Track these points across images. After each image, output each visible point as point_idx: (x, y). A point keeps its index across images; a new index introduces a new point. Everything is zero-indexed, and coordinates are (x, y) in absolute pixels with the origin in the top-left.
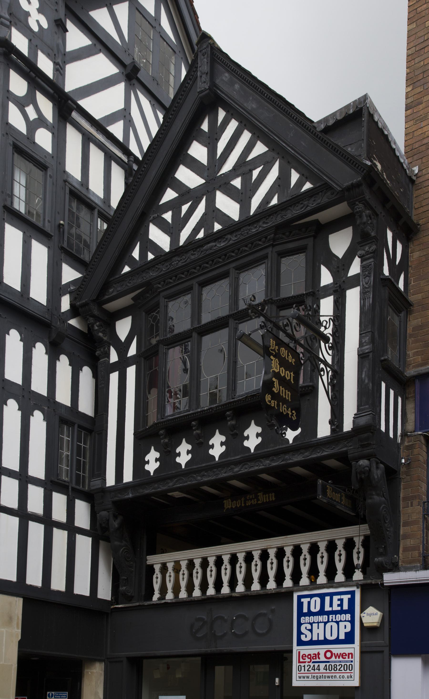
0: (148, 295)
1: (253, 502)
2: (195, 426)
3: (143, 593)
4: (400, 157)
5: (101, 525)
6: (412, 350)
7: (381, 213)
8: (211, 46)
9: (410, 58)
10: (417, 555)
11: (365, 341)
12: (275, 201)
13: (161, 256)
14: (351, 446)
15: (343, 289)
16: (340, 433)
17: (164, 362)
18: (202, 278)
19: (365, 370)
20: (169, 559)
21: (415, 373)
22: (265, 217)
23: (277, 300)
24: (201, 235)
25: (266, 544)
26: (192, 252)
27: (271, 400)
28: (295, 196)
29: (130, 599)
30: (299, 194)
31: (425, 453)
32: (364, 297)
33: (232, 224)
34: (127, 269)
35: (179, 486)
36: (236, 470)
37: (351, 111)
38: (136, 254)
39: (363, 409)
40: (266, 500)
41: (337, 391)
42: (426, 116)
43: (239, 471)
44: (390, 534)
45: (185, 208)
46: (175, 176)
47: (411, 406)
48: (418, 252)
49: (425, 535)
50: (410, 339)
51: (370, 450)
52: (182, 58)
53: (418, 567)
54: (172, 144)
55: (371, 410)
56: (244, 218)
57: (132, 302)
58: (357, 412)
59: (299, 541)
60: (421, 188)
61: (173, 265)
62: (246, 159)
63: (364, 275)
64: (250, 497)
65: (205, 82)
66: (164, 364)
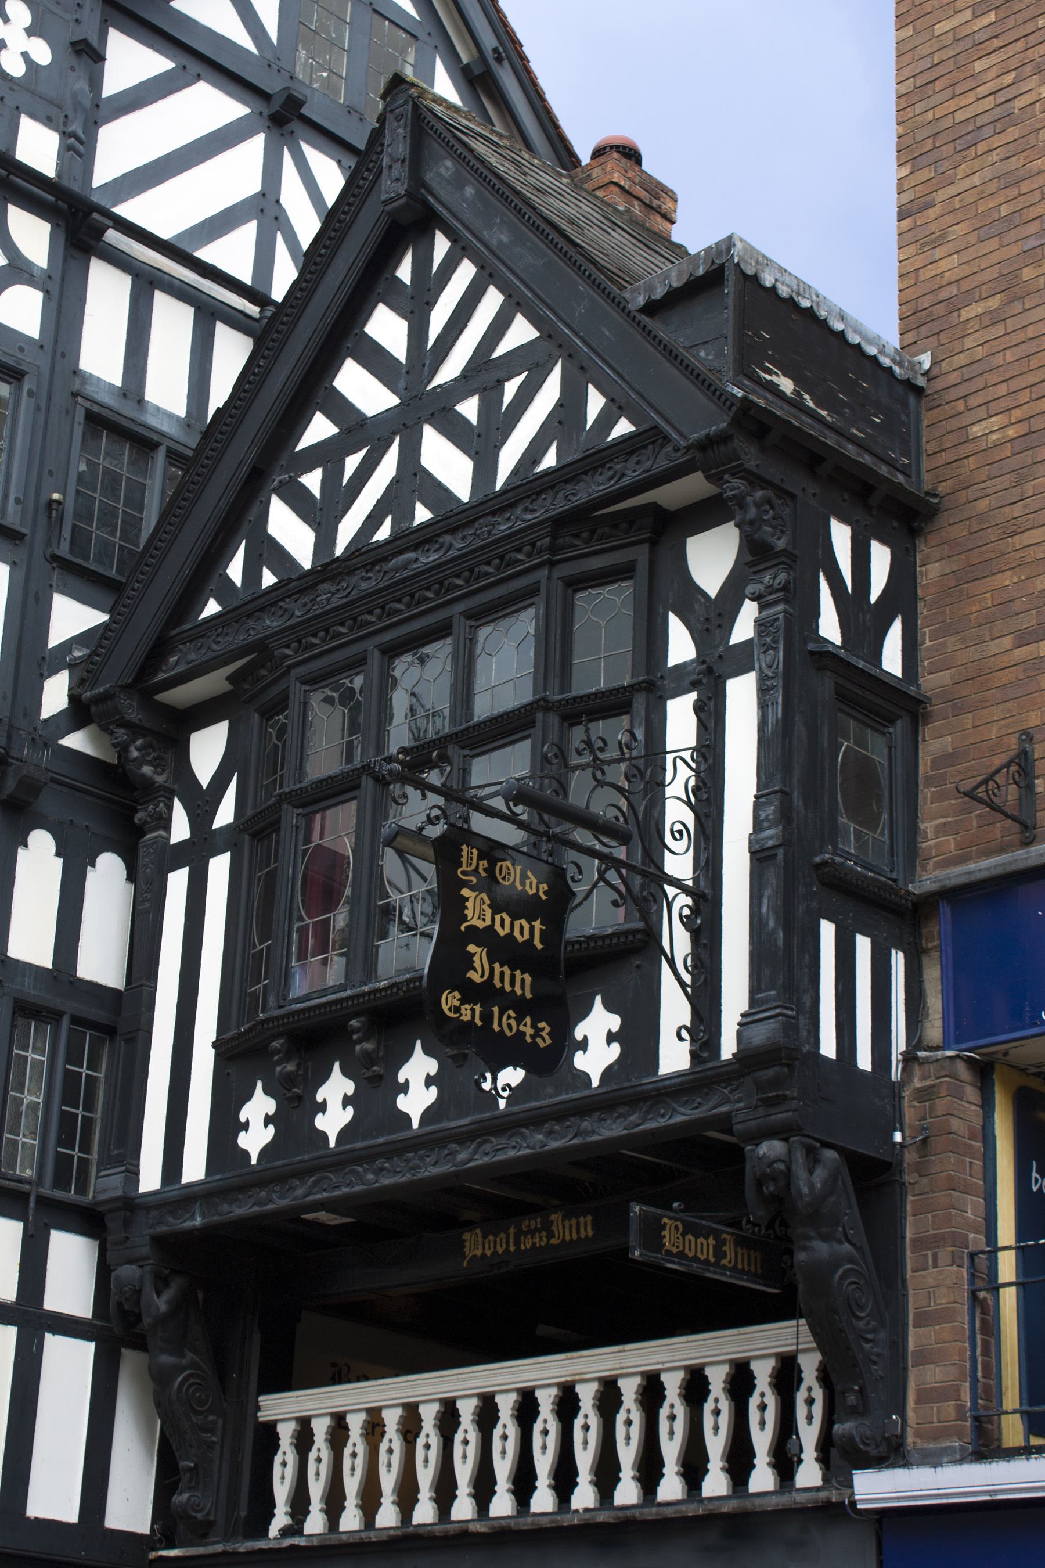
0: (264, 672)
1: (538, 1240)
2: (358, 1030)
3: (243, 1514)
4: (864, 345)
5: (120, 1304)
6: (932, 819)
7: (804, 490)
8: (414, 103)
9: (905, 102)
10: (953, 1414)
11: (767, 816)
12: (550, 460)
13: (290, 580)
14: (739, 1101)
15: (720, 676)
16: (710, 1065)
17: (293, 851)
18: (387, 637)
19: (768, 892)
20: (316, 1406)
21: (933, 885)
22: (528, 497)
23: (560, 701)
24: (384, 533)
25: (571, 1370)
26: (364, 574)
27: (462, 1004)
28: (591, 451)
29: (202, 1532)
30: (603, 446)
31: (973, 1108)
32: (765, 700)
33: (451, 511)
34: (212, 608)
35: (320, 1199)
36: (462, 1156)
37: (701, 271)
38: (235, 571)
39: (765, 1001)
40: (571, 1234)
41: (705, 946)
42: (943, 236)
43: (470, 1160)
44: (875, 1350)
45: (352, 463)
46: (334, 384)
47: (932, 975)
48: (937, 564)
49: (978, 1352)
50: (926, 790)
51: (785, 1115)
52: (436, 47)
53: (955, 1452)
54: (325, 313)
55: (779, 1003)
56: (480, 497)
57: (227, 687)
58: (750, 1007)
59: (655, 1361)
60: (940, 405)
61: (318, 604)
62: (491, 355)
63: (764, 645)
64: (529, 1226)
65: (397, 180)
66: (292, 856)
